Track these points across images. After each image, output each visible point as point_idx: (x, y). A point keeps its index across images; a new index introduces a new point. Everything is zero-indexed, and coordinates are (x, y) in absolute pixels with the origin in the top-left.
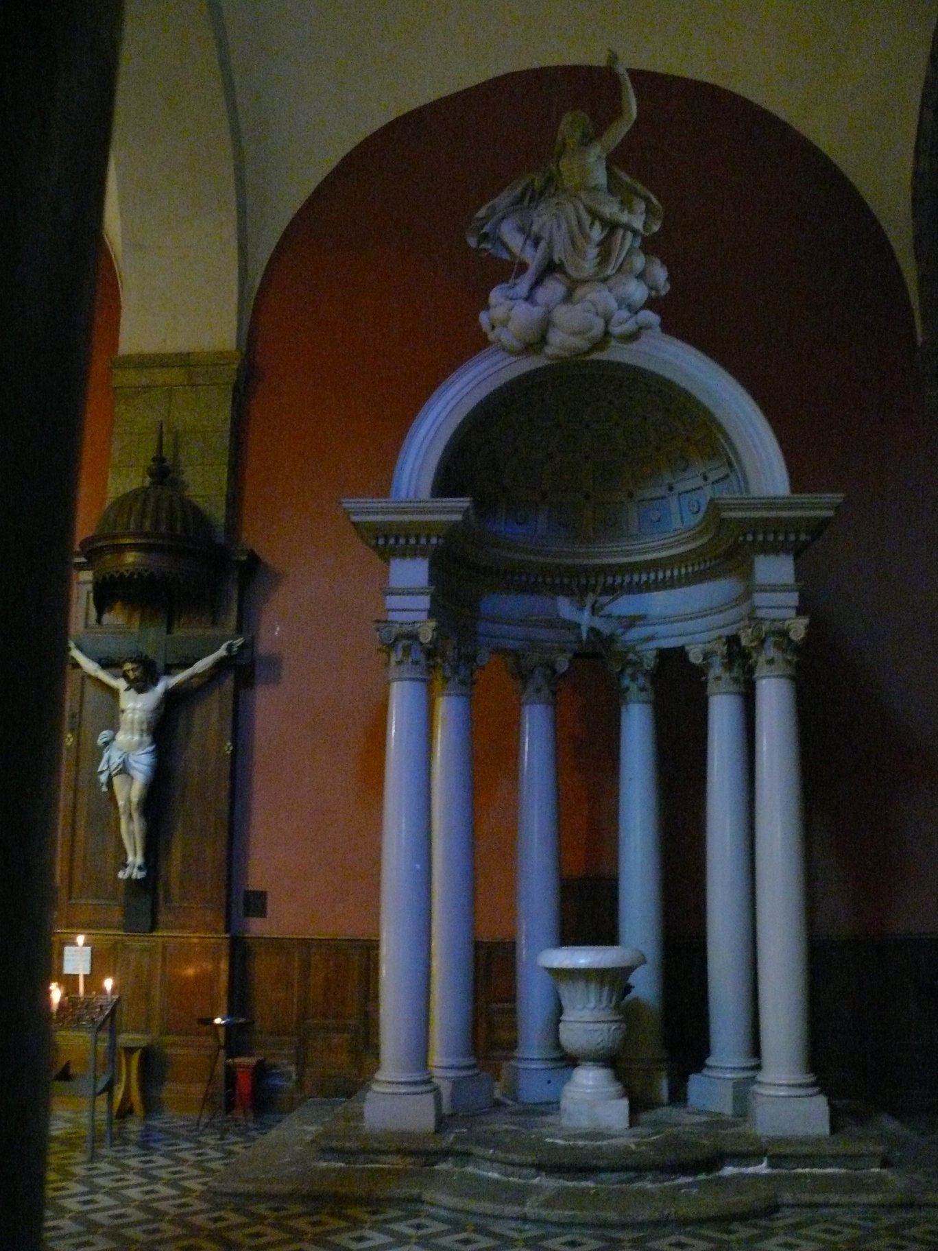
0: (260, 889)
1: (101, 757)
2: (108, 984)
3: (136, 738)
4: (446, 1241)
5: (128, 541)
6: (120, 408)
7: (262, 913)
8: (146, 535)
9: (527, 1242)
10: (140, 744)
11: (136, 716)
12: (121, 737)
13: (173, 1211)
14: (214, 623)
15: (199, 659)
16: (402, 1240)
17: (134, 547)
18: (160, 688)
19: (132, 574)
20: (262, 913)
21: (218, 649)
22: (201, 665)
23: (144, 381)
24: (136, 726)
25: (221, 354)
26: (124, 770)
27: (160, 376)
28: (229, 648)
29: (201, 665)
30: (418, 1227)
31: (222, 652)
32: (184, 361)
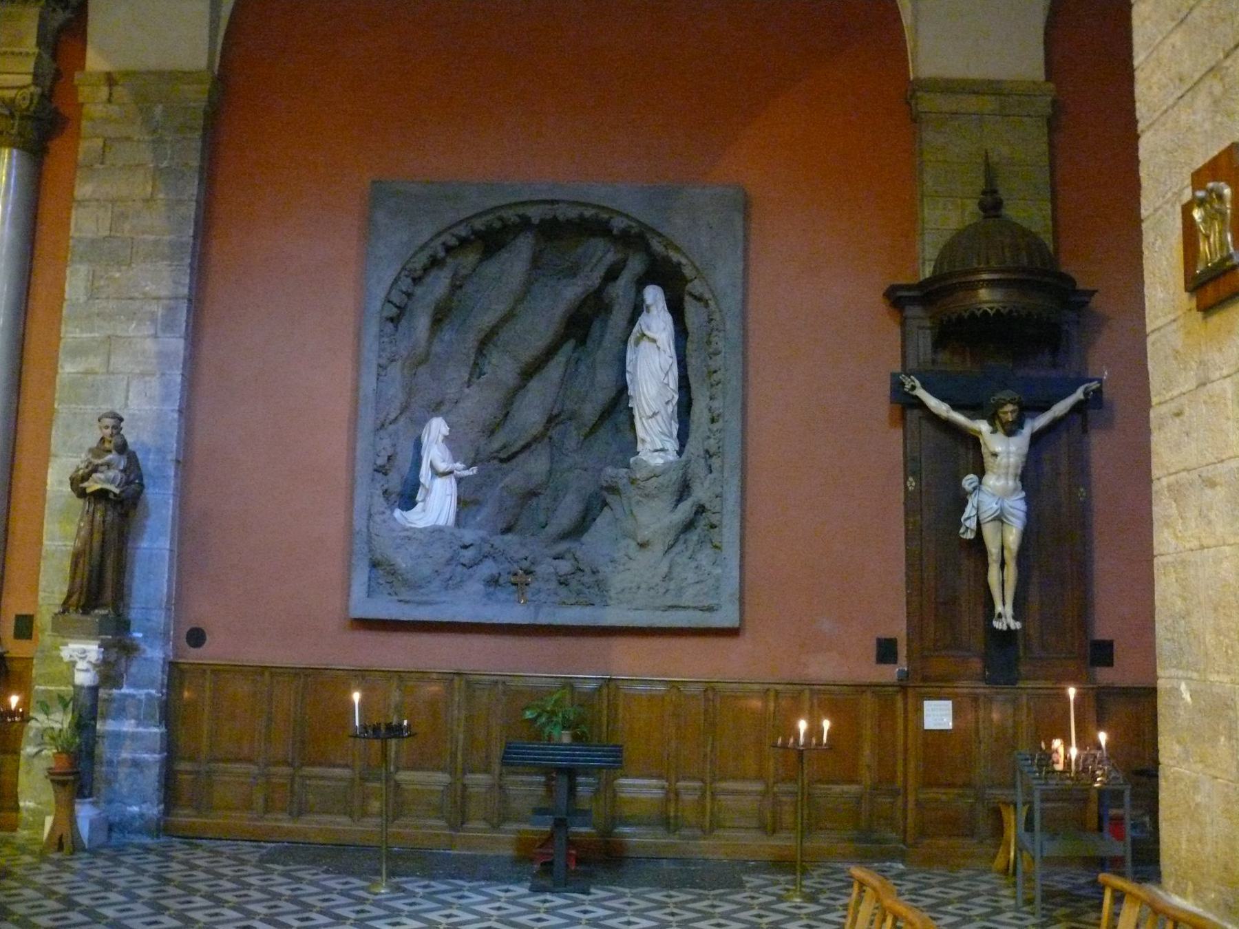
0: (1107, 638)
1: (965, 503)
2: (1103, 737)
3: (1011, 483)
4: (523, 920)
5: (985, 276)
6: (929, 135)
7: (1110, 664)
8: (1008, 270)
9: (590, 922)
10: (1015, 489)
11: (1012, 460)
12: (991, 481)
13: (274, 877)
14: (1054, 366)
15: (1057, 401)
16: (574, 921)
17: (990, 284)
18: (1027, 431)
19: (1011, 311)
20: (1110, 664)
21: (1074, 391)
22: (1061, 408)
23: (954, 108)
24: (1011, 470)
25: (198, 72)
26: (1000, 519)
27: (971, 103)
28: (1086, 393)
29: (1061, 408)
30: (499, 909)
31: (1079, 395)
32: (993, 88)
